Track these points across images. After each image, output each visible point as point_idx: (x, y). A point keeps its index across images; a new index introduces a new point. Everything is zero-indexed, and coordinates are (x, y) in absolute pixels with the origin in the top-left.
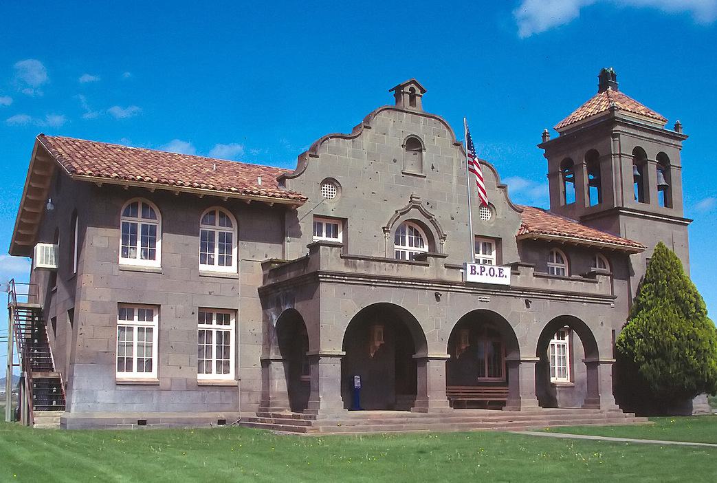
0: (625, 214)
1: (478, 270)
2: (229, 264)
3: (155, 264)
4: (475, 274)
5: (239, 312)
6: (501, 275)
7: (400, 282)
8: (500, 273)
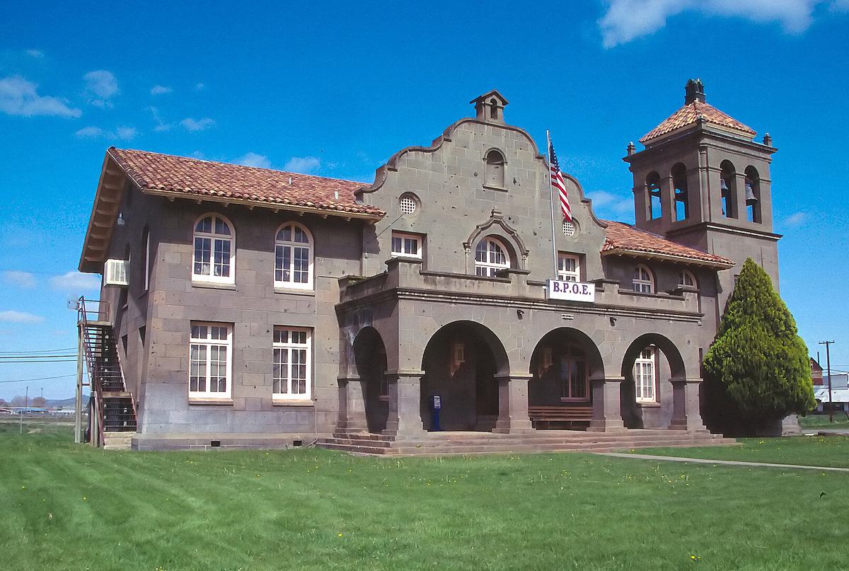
1: (561, 287)
2: (305, 281)
3: (229, 281)
4: (558, 291)
6: (585, 292)
7: (481, 300)
8: (584, 290)
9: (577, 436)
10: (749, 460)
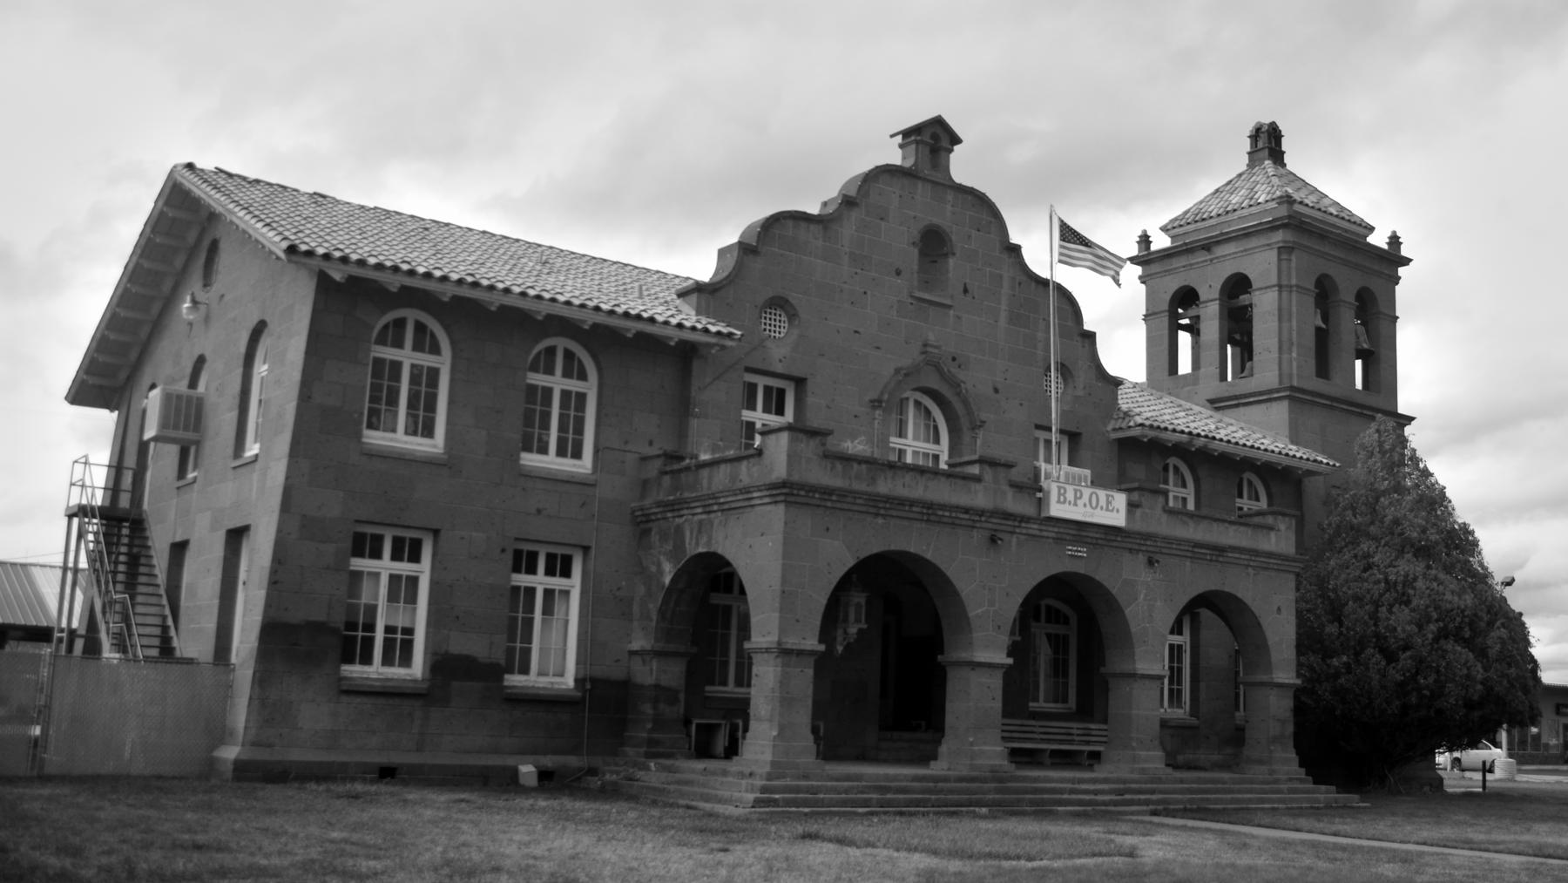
0: (1278, 391)
1: (1070, 496)
2: (577, 455)
3: (435, 445)
4: (1064, 502)
5: (593, 552)
6: (1110, 508)
7: (930, 512)
8: (1108, 503)
9: (1081, 781)
10: (1415, 838)
